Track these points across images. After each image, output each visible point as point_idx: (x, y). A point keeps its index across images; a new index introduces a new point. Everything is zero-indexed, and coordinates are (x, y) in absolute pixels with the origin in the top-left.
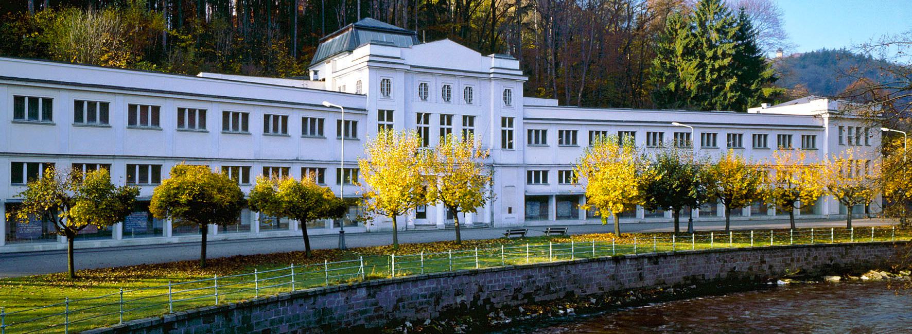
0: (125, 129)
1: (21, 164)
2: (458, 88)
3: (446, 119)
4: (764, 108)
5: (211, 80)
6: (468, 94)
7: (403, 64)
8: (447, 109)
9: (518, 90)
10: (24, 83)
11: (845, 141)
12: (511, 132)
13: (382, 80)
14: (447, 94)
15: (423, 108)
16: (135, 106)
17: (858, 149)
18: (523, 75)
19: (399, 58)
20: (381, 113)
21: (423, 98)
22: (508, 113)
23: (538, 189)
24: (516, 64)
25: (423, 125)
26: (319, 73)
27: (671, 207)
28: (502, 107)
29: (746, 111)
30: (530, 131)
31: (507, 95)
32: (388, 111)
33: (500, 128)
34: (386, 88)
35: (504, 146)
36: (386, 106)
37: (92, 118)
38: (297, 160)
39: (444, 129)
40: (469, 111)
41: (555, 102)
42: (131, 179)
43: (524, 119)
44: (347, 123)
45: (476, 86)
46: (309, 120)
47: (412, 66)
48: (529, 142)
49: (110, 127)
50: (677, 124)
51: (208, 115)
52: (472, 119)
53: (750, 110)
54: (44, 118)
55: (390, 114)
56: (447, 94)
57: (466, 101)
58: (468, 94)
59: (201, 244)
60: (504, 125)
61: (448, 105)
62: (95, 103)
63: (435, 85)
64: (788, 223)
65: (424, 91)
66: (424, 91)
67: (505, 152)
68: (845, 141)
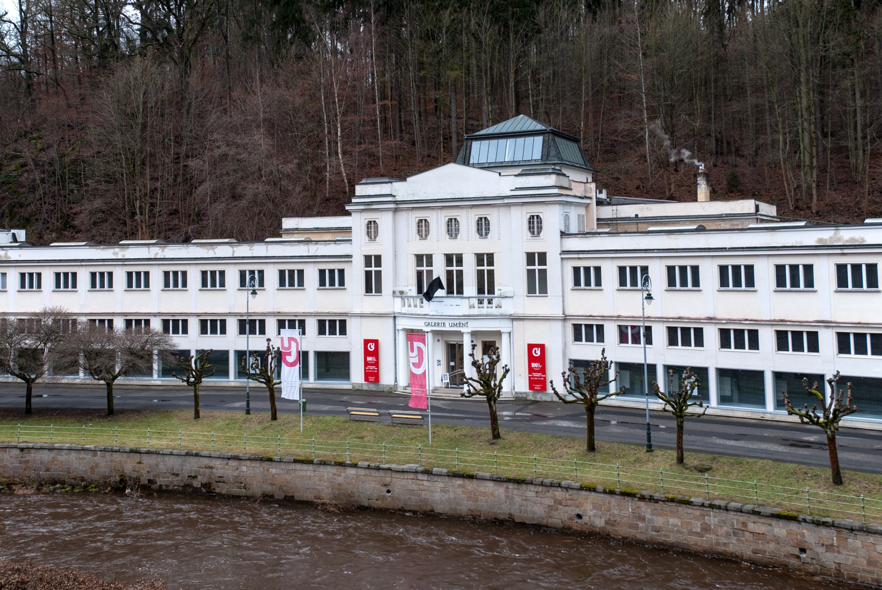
0: (615, 291)
1: (206, 320)
2: (467, 220)
6: (483, 227)
8: (453, 247)
10: (576, 256)
14: (452, 228)
15: (423, 248)
16: (625, 268)
20: (368, 259)
22: (536, 247)
23: (589, 352)
28: (525, 239)
32: (539, 253)
37: (857, 283)
38: (714, 318)
40: (484, 246)
42: (166, 329)
44: (102, 274)
45: (493, 215)
46: (62, 275)
49: (815, 291)
54: (869, 286)
55: (378, 258)
56: (452, 228)
58: (483, 227)
61: (453, 242)
62: (169, 272)
63: (437, 220)
64: (642, 429)
65: (423, 228)
66: (423, 228)
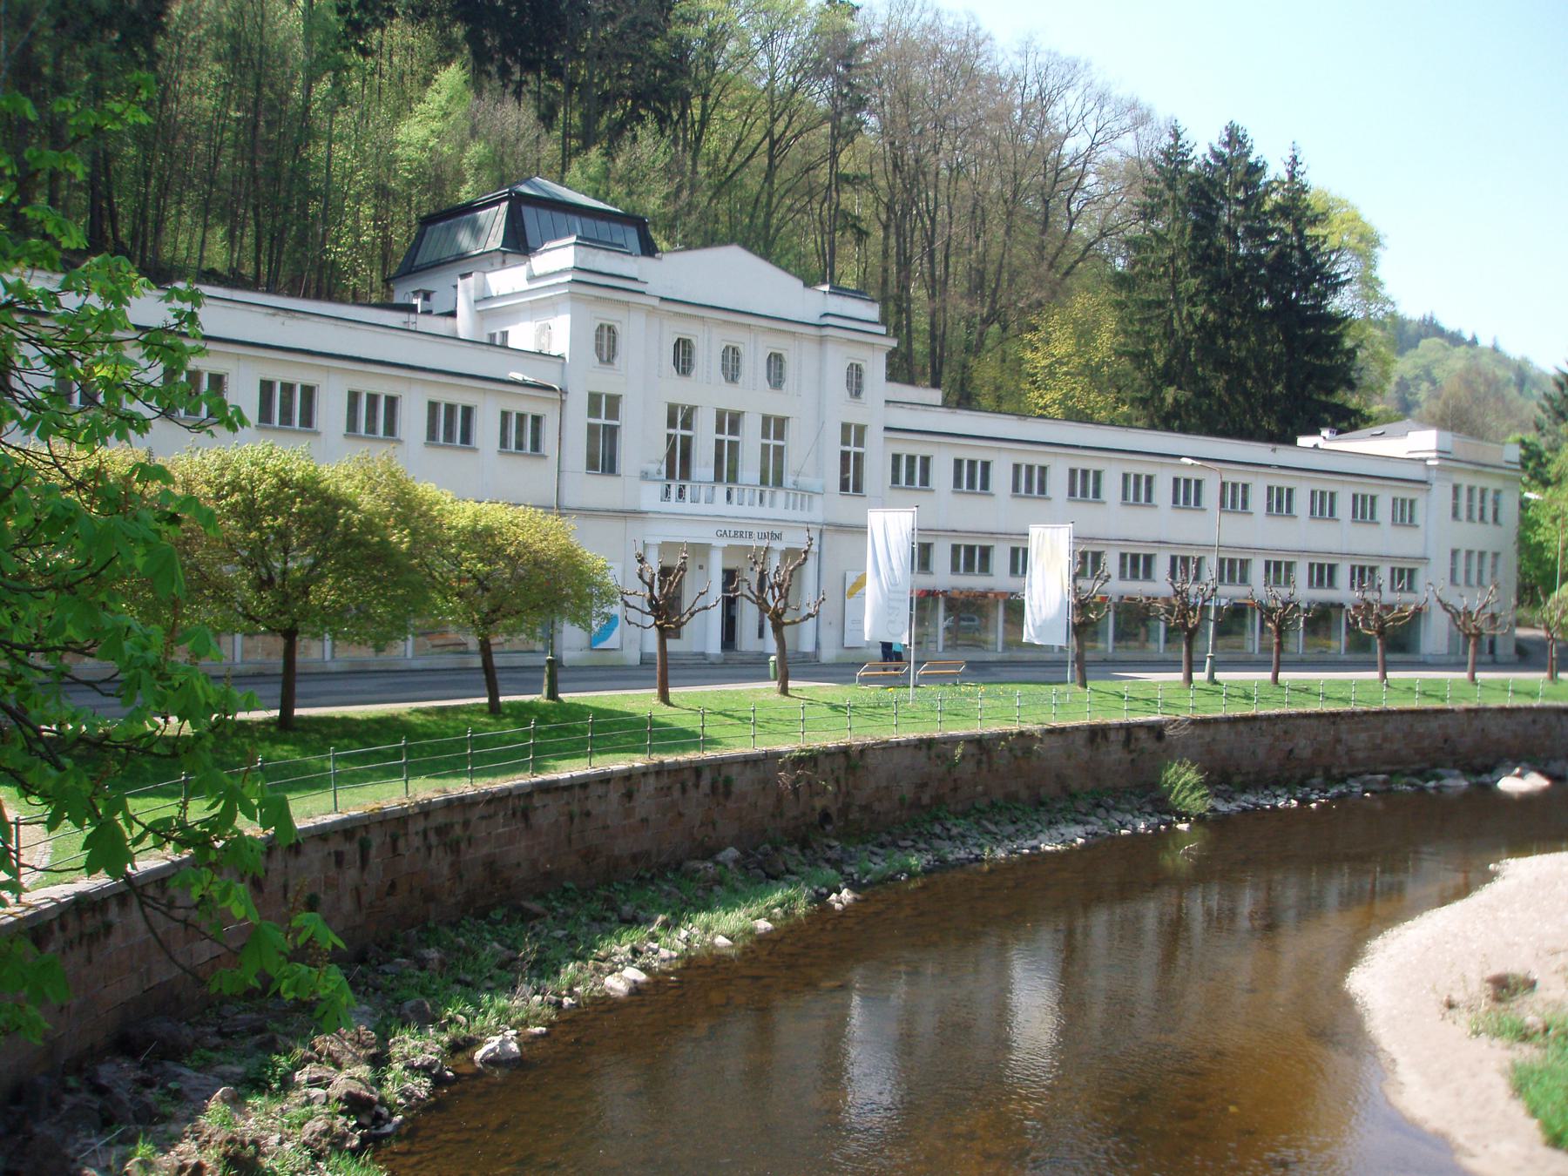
3: (730, 421)
4: (1324, 439)
5: (1411, 485)
7: (643, 293)
9: (876, 369)
11: (1463, 513)
12: (734, 446)
13: (597, 325)
14: (731, 364)
17: (1478, 526)
18: (886, 335)
19: (635, 279)
21: (605, 358)
24: (872, 311)
25: (679, 432)
26: (434, 297)
27: (66, 814)
29: (1293, 442)
30: (896, 458)
31: (855, 380)
33: (839, 448)
34: (606, 344)
35: (844, 486)
36: (606, 382)
39: (849, 453)
40: (776, 404)
41: (936, 396)
43: (887, 429)
47: (663, 299)
48: (895, 479)
50: (1190, 461)
51: (1251, 491)
52: (781, 423)
53: (1303, 441)
56: (731, 364)
57: (851, 391)
59: (280, 679)
60: (672, 423)
67: (1270, 519)
68: (1463, 513)
